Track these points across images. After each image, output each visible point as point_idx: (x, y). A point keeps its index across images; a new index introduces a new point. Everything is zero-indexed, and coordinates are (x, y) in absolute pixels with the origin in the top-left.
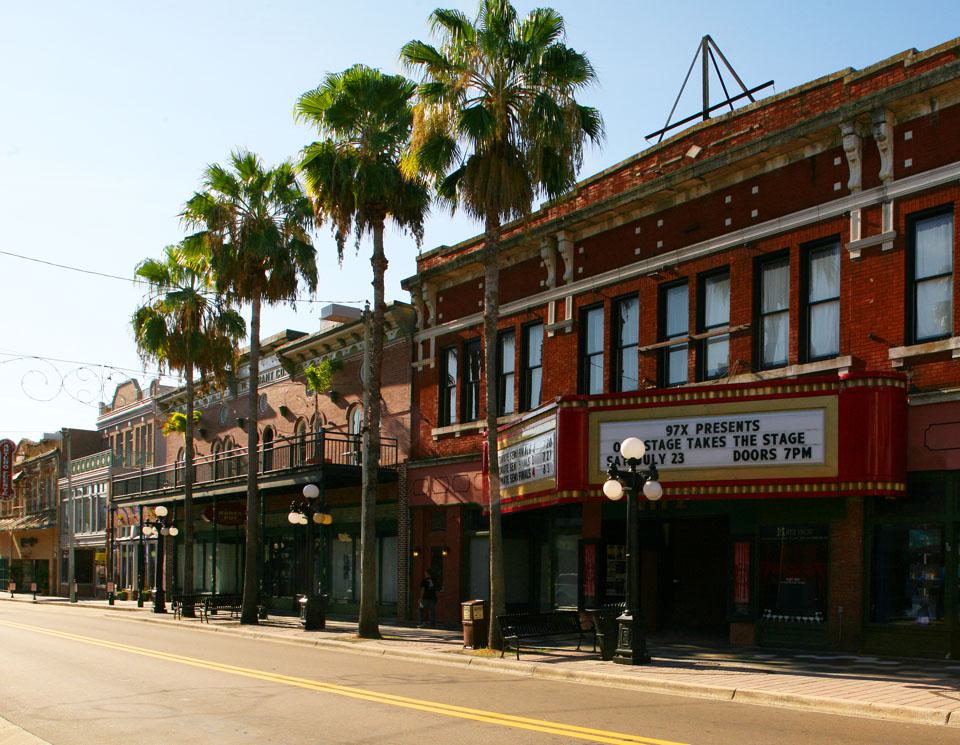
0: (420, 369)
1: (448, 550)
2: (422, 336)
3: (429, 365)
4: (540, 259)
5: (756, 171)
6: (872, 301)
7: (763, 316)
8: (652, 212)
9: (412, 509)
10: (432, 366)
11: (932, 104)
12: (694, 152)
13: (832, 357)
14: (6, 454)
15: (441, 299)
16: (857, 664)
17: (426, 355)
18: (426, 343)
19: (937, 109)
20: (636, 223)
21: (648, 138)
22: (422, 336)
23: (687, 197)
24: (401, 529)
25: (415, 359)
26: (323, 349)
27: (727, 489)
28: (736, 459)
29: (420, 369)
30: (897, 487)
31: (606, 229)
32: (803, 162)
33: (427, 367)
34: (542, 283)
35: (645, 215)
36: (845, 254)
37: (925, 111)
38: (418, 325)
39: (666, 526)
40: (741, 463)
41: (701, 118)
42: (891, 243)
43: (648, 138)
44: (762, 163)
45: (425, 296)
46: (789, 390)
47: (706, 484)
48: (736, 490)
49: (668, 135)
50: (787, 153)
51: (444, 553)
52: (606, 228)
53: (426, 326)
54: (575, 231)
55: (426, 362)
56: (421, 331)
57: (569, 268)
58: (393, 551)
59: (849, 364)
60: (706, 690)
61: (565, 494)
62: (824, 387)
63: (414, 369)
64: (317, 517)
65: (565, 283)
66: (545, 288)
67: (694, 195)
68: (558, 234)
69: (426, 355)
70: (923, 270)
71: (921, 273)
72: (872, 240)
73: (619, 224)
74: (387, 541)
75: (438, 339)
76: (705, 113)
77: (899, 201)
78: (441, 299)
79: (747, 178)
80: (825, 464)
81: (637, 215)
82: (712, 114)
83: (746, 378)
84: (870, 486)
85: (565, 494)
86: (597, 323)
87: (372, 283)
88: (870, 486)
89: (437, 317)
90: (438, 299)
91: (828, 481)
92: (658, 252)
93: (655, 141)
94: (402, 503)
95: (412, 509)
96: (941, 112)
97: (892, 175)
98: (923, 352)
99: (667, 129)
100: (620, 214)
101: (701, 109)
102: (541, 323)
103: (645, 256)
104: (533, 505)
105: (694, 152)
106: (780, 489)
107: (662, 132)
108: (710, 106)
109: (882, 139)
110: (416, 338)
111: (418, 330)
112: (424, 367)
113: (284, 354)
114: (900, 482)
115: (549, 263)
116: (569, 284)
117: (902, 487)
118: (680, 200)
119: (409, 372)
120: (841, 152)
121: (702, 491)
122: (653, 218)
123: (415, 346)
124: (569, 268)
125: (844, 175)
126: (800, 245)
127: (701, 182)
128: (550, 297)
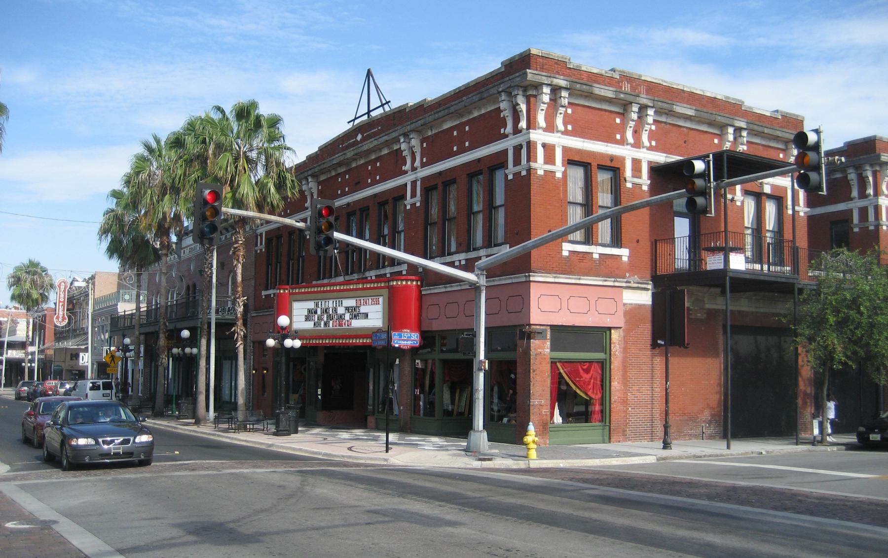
8: (344, 170)
10: (418, 204)
14: (62, 291)
15: (425, 145)
18: (261, 235)
21: (349, 122)
22: (259, 231)
25: (256, 245)
34: (502, 131)
36: (506, 176)
37: (430, 133)
42: (419, 203)
43: (349, 122)
49: (357, 122)
66: (506, 136)
75: (267, 233)
77: (424, 180)
78: (425, 145)
82: (373, 114)
90: (318, 188)
96: (435, 134)
99: (356, 118)
101: (367, 111)
107: (353, 120)
108: (371, 109)
112: (514, 174)
115: (507, 114)
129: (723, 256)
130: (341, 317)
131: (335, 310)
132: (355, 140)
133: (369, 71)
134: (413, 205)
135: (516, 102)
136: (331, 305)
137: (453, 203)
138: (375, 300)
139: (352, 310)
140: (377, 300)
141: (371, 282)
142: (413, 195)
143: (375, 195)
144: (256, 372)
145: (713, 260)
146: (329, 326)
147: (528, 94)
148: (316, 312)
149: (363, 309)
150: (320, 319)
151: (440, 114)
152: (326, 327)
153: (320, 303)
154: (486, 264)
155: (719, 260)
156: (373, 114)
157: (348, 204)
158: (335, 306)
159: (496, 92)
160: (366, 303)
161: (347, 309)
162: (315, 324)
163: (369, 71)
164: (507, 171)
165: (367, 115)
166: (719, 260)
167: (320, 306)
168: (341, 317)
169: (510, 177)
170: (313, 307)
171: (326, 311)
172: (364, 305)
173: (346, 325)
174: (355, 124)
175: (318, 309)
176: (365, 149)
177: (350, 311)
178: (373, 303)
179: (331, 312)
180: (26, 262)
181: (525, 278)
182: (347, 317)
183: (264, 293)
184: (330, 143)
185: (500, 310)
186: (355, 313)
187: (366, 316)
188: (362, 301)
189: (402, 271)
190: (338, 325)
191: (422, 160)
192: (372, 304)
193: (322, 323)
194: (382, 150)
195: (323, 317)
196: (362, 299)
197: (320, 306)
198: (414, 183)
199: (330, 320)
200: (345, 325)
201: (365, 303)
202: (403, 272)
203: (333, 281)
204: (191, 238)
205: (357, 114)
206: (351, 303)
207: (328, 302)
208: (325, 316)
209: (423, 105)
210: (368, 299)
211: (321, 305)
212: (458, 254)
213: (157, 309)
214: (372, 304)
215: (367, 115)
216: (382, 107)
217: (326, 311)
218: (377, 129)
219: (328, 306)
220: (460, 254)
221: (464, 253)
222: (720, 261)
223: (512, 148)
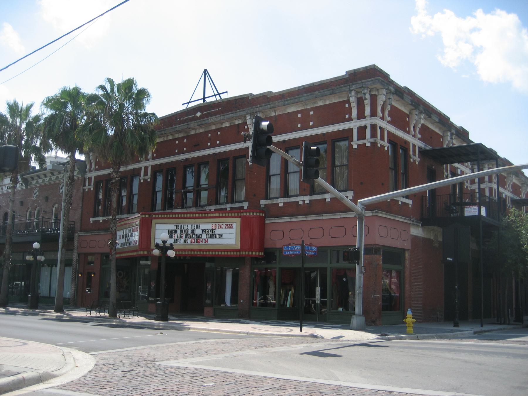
0: (87, 190)
1: (94, 274)
2: (88, 175)
3: (91, 189)
5: (219, 126)
6: (255, 182)
7: (270, 176)
8: (183, 136)
9: (79, 254)
11: (275, 112)
12: (199, 114)
13: (277, 198)
16: (284, 324)
17: (90, 184)
18: (90, 179)
19: (277, 114)
20: (177, 139)
22: (88, 175)
23: (196, 132)
24: (74, 263)
25: (84, 185)
26: (43, 176)
27: (180, 252)
29: (87, 190)
30: (260, 254)
31: (165, 140)
32: (234, 125)
33: (89, 189)
35: (179, 136)
36: (140, 180)
37: (273, 114)
39: (186, 265)
41: (202, 101)
43: (183, 104)
44: (222, 124)
45: (91, 158)
46: (191, 215)
47: (228, 251)
48: (196, 253)
50: (230, 121)
51: (93, 275)
53: (91, 171)
55: (89, 187)
56: (88, 172)
57: (93, 166)
58: (69, 272)
59: (247, 205)
61: (142, 253)
62: (224, 215)
63: (84, 190)
64: (39, 257)
65: (148, 160)
67: (198, 132)
68: (247, 115)
69: (90, 184)
70: (134, 193)
71: (289, 171)
72: (362, 142)
73: (170, 139)
74: (67, 269)
76: (204, 98)
79: (216, 128)
80: (236, 245)
81: (177, 136)
83: (307, 199)
84: (250, 253)
85: (142, 253)
88: (254, 253)
89: (96, 167)
90: (96, 160)
91: (236, 251)
92: (183, 152)
93: (185, 106)
94: (75, 251)
95: (79, 254)
96: (278, 115)
97: (370, 115)
98: (270, 203)
99: (190, 102)
100: (171, 135)
101: (220, 93)
104: (141, 254)
105: (199, 114)
106: (204, 253)
107: (188, 103)
108: (206, 97)
109: (366, 99)
110: (86, 176)
111: (87, 172)
112: (88, 189)
113: (24, 177)
114: (262, 252)
116: (143, 162)
117: (262, 254)
118: (193, 132)
119: (81, 191)
120: (348, 102)
121: (192, 253)
122: (183, 138)
123: (85, 179)
124: (93, 166)
125: (350, 113)
126: (218, 160)
127: (200, 127)
129: (477, 208)
130: (198, 236)
131: (194, 231)
132: (194, 116)
133: (205, 71)
134: (89, 189)
135: (365, 98)
136: (190, 227)
137: (101, 191)
138: (228, 225)
139: (208, 232)
140: (231, 225)
141: (213, 213)
142: (146, 174)
143: (216, 154)
144: (81, 275)
145: (474, 210)
146: (187, 243)
147: (372, 94)
148: (176, 232)
149: (218, 231)
150: (179, 237)
151: (290, 101)
152: (185, 243)
153: (180, 226)
154: (371, 201)
155: (475, 210)
156: (208, 100)
157: (186, 160)
158: (193, 228)
159: (348, 90)
160: (221, 227)
161: (204, 231)
162: (175, 241)
163: (205, 71)
164: (140, 178)
165: (202, 100)
166: (475, 210)
167: (180, 228)
168: (198, 236)
169: (142, 181)
170: (174, 229)
171: (185, 231)
172: (219, 228)
173: (203, 242)
174: (188, 107)
175: (178, 230)
176: (210, 122)
177: (206, 232)
178: (227, 227)
179: (189, 232)
180: (72, 87)
181: (371, 214)
182: (204, 236)
183: (92, 219)
184: (167, 117)
185: (283, 238)
186: (211, 234)
187: (221, 236)
188: (217, 226)
189: (243, 207)
190: (195, 242)
191: (153, 155)
192: (226, 228)
193: (182, 240)
194: (224, 124)
195: (182, 236)
196: (217, 224)
197: (180, 228)
198: (146, 168)
199: (189, 238)
200: (202, 242)
201: (219, 227)
202: (101, 221)
203: (174, 211)
204: (9, 179)
205: (192, 99)
206: (209, 227)
207: (188, 225)
208: (184, 235)
209: (267, 95)
210: (223, 225)
211: (181, 227)
212: (303, 197)
213: (13, 225)
214: (226, 228)
216: (220, 95)
217: (185, 231)
218: (217, 110)
219: (187, 228)
220: (305, 196)
221: (230, 204)
222: (476, 211)
223: (357, 128)
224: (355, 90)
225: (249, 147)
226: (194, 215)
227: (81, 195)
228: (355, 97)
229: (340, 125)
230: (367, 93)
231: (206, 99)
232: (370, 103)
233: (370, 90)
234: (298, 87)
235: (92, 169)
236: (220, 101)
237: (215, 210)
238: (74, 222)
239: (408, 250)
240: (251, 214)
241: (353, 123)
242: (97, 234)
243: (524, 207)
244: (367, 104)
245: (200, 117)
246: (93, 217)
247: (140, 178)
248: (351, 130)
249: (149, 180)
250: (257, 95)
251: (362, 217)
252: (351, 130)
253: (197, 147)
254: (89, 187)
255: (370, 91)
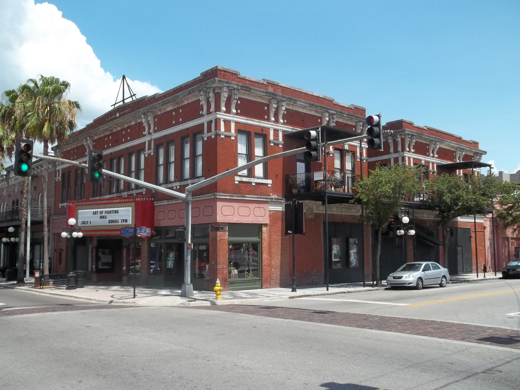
0: (57, 181)
2: (58, 168)
4: (199, 101)
9: (54, 234)
10: (152, 154)
15: (156, 120)
18: (59, 171)
21: (112, 106)
22: (58, 168)
23: (116, 130)
25: (56, 177)
28: (109, 223)
34: (201, 112)
36: (203, 138)
37: (159, 113)
38: (56, 164)
40: (111, 224)
43: (112, 106)
49: (116, 106)
52: (100, 137)
54: (92, 137)
56: (153, 134)
60: (76, 297)
63: (56, 180)
65: (211, 113)
75: (62, 169)
78: (156, 120)
82: (125, 101)
86: (162, 152)
87: (217, 67)
90: (93, 144)
95: (54, 234)
96: (162, 114)
99: (116, 104)
101: (122, 100)
102: (201, 133)
103: (176, 124)
107: (114, 105)
108: (125, 98)
110: (56, 169)
111: (57, 166)
112: (148, 154)
115: (203, 103)
118: (114, 131)
119: (54, 181)
122: (109, 135)
123: (56, 171)
128: (146, 139)
134: (149, 154)
156: (126, 101)
164: (203, 136)
165: (122, 102)
169: (205, 139)
183: (60, 205)
191: (154, 128)
194: (131, 122)
198: (150, 142)
202: (174, 187)
203: (102, 198)
204: (13, 173)
215: (122, 102)
224: (203, 90)
225: (145, 142)
226: (108, 202)
227: (54, 185)
228: (205, 95)
229: (197, 120)
230: (210, 92)
231: (125, 101)
232: (214, 100)
233: (213, 89)
234: (174, 89)
235: (151, 131)
236: (136, 101)
237: (128, 195)
238: (50, 207)
239: (266, 225)
240: (147, 199)
241: (212, 115)
242: (62, 217)
243: (461, 170)
244: (211, 101)
245: (119, 117)
246: (61, 203)
247: (203, 136)
248: (203, 124)
249: (152, 154)
250: (151, 96)
251: (188, 201)
252: (203, 124)
253: (117, 142)
254: (209, 134)
255: (214, 90)
